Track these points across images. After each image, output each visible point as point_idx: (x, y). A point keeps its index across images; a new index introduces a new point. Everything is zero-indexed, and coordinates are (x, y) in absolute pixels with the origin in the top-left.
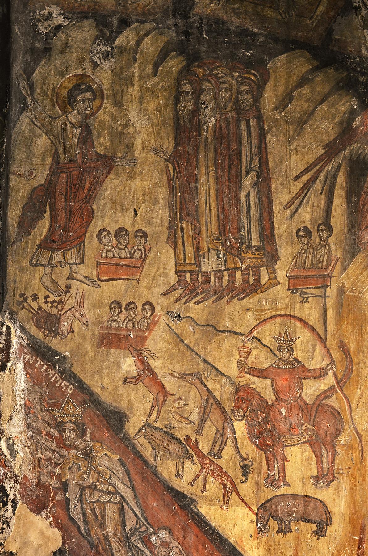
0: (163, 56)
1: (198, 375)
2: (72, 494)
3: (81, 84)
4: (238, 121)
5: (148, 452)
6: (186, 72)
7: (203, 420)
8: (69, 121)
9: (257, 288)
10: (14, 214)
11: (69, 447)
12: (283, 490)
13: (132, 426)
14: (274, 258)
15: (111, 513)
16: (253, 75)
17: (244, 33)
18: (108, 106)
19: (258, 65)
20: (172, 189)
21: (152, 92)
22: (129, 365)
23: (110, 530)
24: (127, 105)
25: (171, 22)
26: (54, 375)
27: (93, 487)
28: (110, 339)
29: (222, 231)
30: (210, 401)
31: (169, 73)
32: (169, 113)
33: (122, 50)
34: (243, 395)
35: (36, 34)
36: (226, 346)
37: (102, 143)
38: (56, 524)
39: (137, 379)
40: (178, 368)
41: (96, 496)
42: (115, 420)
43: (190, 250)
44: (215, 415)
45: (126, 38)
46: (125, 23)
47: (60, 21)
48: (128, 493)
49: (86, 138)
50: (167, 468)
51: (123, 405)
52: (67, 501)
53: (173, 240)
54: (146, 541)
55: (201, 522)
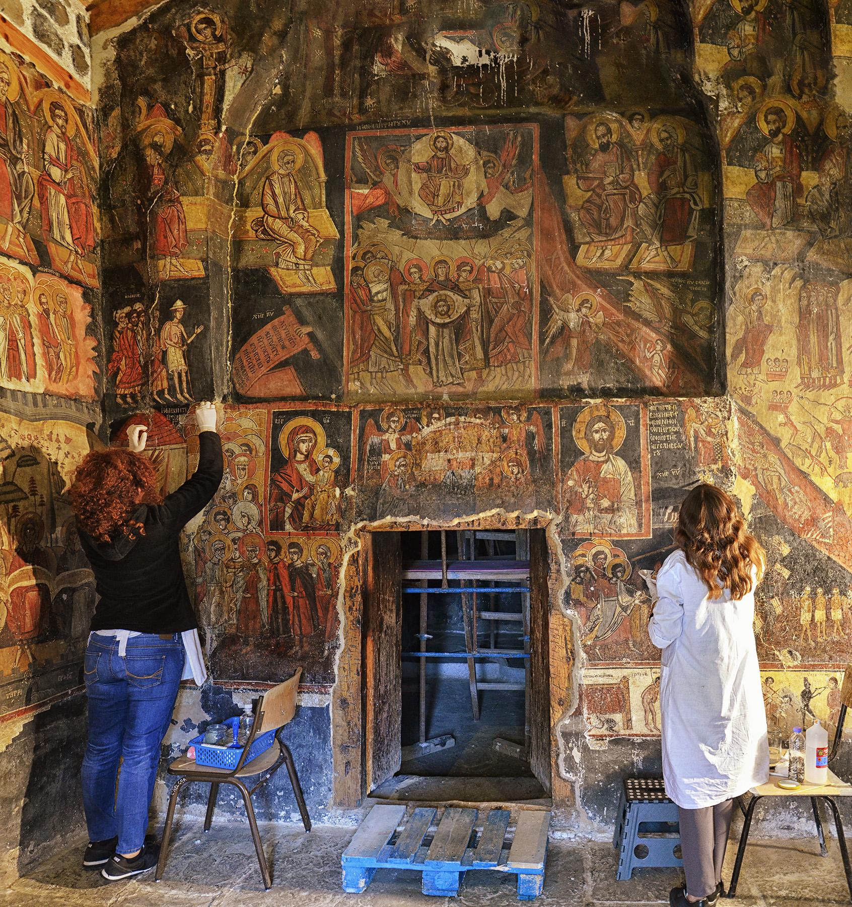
0: (793, 280)
1: (810, 423)
2: (759, 472)
3: (757, 292)
4: (827, 310)
5: (790, 455)
6: (804, 287)
7: (813, 442)
8: (235, 772)
9: (835, 385)
10: (729, 352)
11: (757, 453)
12: (845, 470)
13: (783, 445)
14: (843, 372)
15: (775, 480)
16: (833, 289)
17: (829, 270)
18: (769, 302)
19: (835, 284)
20: (799, 341)
21: (789, 296)
22: (781, 418)
23: (775, 487)
24: (778, 302)
25: (796, 264)
26: (750, 422)
27: (767, 469)
28: (773, 407)
29: (821, 360)
30: (816, 434)
31: (796, 287)
32: (796, 306)
33: (775, 277)
34: (829, 431)
35: (736, 269)
36: (822, 410)
37: (767, 319)
38: (753, 484)
39: (785, 424)
40: (802, 420)
41: (769, 473)
42: (776, 442)
43: (806, 368)
44: (818, 439)
45: (776, 271)
46: (775, 264)
47: (746, 263)
48: (782, 472)
49: (760, 317)
50: (798, 462)
51: (779, 435)
52: (757, 475)
53: (799, 364)
54: (790, 491)
55: (812, 483)
